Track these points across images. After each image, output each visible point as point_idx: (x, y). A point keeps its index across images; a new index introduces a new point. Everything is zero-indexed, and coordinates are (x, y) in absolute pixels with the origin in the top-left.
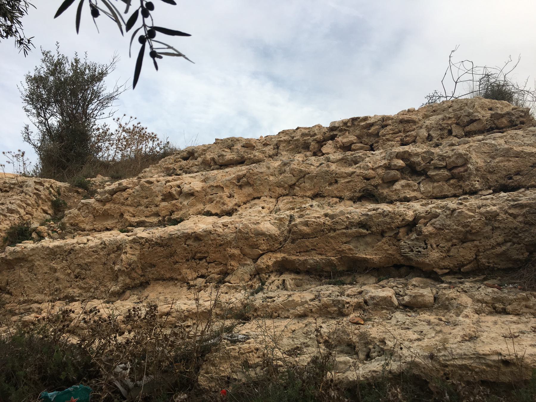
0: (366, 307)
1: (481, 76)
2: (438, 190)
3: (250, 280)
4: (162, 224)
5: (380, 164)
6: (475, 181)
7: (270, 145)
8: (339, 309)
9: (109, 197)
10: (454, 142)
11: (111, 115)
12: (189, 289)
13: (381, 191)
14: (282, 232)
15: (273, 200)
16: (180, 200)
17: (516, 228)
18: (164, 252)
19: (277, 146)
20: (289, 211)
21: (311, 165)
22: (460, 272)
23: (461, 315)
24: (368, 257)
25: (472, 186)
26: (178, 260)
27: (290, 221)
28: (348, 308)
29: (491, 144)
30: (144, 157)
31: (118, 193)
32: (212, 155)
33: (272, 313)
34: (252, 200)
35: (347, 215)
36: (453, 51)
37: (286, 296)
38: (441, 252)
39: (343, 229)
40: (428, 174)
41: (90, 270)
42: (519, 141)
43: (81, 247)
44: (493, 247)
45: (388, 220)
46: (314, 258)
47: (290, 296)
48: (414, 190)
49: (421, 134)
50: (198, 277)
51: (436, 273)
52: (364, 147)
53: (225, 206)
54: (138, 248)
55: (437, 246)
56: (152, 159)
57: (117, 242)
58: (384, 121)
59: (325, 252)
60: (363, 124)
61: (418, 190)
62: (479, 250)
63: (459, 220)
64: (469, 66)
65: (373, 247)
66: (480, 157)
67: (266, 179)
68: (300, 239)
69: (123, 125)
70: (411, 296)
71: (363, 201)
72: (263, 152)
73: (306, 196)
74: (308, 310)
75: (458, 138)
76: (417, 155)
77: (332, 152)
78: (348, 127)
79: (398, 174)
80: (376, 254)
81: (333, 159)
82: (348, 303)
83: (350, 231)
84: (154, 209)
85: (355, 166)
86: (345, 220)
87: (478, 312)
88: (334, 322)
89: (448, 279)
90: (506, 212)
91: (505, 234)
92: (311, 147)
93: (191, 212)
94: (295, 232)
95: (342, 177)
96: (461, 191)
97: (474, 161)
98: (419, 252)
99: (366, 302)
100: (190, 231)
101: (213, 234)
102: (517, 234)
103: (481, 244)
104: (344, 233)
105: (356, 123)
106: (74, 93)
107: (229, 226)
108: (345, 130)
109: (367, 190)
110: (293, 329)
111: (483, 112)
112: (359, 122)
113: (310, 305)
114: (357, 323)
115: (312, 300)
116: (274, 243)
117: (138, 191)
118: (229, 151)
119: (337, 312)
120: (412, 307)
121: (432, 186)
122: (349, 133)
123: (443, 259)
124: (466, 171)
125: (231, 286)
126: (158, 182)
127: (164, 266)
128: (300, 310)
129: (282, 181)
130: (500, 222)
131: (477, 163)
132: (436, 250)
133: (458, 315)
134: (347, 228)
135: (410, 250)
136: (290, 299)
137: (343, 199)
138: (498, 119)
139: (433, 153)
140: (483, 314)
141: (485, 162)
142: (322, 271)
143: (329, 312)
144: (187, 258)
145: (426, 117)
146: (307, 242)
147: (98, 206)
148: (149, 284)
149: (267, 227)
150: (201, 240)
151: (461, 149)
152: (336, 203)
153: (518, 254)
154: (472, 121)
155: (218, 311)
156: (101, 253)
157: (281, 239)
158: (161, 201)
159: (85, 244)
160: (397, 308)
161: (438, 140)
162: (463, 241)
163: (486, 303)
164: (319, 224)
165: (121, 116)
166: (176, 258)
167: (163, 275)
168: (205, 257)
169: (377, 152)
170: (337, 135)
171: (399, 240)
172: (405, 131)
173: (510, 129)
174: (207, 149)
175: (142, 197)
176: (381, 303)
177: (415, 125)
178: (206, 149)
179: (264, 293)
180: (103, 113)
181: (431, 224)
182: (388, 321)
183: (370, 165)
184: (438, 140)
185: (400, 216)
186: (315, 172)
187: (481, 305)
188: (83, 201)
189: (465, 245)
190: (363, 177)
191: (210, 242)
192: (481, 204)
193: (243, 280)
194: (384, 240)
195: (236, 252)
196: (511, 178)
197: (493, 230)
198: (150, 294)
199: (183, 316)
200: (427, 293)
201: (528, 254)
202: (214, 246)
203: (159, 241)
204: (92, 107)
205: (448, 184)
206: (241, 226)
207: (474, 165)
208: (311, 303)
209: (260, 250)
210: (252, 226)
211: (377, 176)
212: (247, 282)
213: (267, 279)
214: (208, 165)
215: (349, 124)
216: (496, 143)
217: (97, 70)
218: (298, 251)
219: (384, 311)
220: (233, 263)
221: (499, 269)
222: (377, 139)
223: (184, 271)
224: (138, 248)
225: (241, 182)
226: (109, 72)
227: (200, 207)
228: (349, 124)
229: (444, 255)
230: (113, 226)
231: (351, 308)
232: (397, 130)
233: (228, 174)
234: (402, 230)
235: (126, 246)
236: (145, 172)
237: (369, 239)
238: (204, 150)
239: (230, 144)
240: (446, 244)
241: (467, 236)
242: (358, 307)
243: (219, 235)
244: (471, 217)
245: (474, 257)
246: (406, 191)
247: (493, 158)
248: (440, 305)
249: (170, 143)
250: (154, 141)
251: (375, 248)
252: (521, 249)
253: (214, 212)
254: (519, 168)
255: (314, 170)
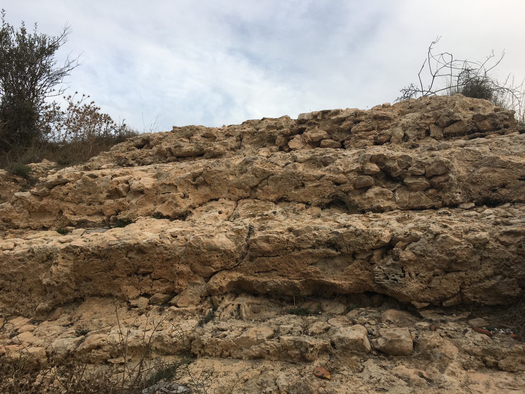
0: (334, 351)
1: (460, 71)
2: (415, 200)
3: (201, 302)
4: (107, 225)
5: (352, 168)
6: (456, 193)
7: (233, 136)
8: (302, 353)
9: (47, 190)
10: (433, 146)
11: (61, 93)
12: (129, 309)
13: (352, 198)
14: (239, 248)
15: (232, 203)
16: (128, 198)
17: (508, 260)
18: (102, 264)
19: (240, 138)
20: (249, 219)
21: (276, 164)
22: (441, 306)
23: (446, 372)
24: (337, 282)
25: (453, 198)
26: (117, 275)
27: (249, 234)
28: (311, 352)
29: (475, 151)
30: (97, 140)
31: (56, 188)
32: (168, 145)
33: (222, 352)
34: (209, 201)
35: (314, 232)
36: (434, 43)
37: (240, 329)
38: (421, 282)
39: (309, 248)
40: (405, 181)
41: (15, 281)
42: (505, 149)
43: (5, 255)
44: (481, 281)
45: (361, 241)
46: (275, 280)
47: (244, 329)
48: (389, 199)
49: (396, 133)
50: (140, 295)
51: (414, 306)
52: (334, 143)
53: (178, 208)
54: (72, 258)
55: (417, 275)
56: (105, 143)
57: (47, 250)
58: (357, 116)
59: (288, 273)
60: (334, 118)
61: (393, 199)
62: (464, 282)
63: (443, 247)
64: (448, 59)
65: (343, 271)
66: (462, 166)
67: (225, 179)
68: (260, 257)
69: (75, 103)
70: (386, 339)
71: (332, 208)
72: (225, 145)
73: (269, 200)
74: (265, 351)
75: (437, 140)
76: (393, 159)
77: (300, 147)
78: (318, 120)
79: (371, 179)
80: (346, 279)
81: (301, 158)
82: (312, 346)
83: (316, 251)
84: (98, 207)
85: (324, 169)
86: (312, 237)
87: (465, 367)
88: (294, 370)
89: (427, 314)
90: (497, 240)
91: (495, 265)
92: (278, 141)
93: (139, 212)
94: (254, 249)
95: (310, 180)
96: (441, 202)
97: (456, 170)
98: (395, 280)
99: (333, 344)
100: (132, 242)
101: (159, 247)
102: (509, 266)
103: (467, 276)
104: (310, 253)
105: (326, 116)
106: (21, 68)
107: (179, 237)
108: (315, 123)
109: (337, 196)
110: (245, 378)
111: (464, 112)
112: (330, 115)
113: (267, 345)
114: (322, 377)
115: (270, 338)
116: (229, 260)
117: (79, 186)
118: (187, 140)
119: (299, 356)
120: (388, 353)
121: (408, 196)
122: (318, 127)
123: (423, 291)
124: (447, 180)
125: (178, 311)
126: (103, 175)
127: (101, 281)
128: (255, 350)
129: (243, 182)
130: (489, 250)
131: (459, 172)
132: (415, 280)
133: (442, 371)
134: (313, 247)
135: (384, 277)
136: (244, 335)
137: (310, 205)
138: (480, 121)
139: (411, 158)
140: (472, 370)
141: (468, 171)
142: (284, 295)
143: (290, 356)
144: (128, 273)
145: (402, 114)
146: (267, 261)
147: (34, 200)
148: (84, 301)
149: (221, 242)
150: (144, 253)
151: (442, 155)
152: (302, 209)
153: (508, 290)
154: (452, 122)
155: (158, 345)
156: (29, 263)
157: (238, 256)
158: (105, 199)
159: (11, 250)
160: (369, 353)
161: (414, 140)
162: (446, 272)
163: (475, 355)
164: (281, 241)
165: (72, 94)
166: (116, 273)
167: (100, 291)
168: (150, 273)
169: (348, 152)
170: (305, 128)
171: (372, 264)
172: (379, 129)
173: (493, 133)
174: (164, 138)
175: (84, 193)
176: (351, 347)
177: (390, 122)
178: (163, 137)
179: (215, 324)
180: (54, 90)
181: (410, 249)
182: (360, 375)
183: (341, 168)
184: (414, 140)
185: (375, 236)
186: (280, 174)
187: (468, 357)
188: (17, 194)
189: (449, 275)
190: (333, 181)
191: (156, 256)
192: (468, 228)
193: (192, 303)
194: (356, 263)
195: (185, 269)
196: (494, 191)
197: (481, 260)
198: (84, 314)
199: (116, 351)
200: (404, 336)
201: (520, 289)
202: (160, 260)
203: (95, 252)
204: (40, 82)
205: (426, 194)
206: (191, 239)
207: (455, 175)
208: (269, 342)
209: (213, 267)
210: (206, 240)
211: (348, 182)
212: (197, 305)
213: (220, 302)
214: (165, 156)
215: (319, 118)
216: (480, 151)
217: (47, 41)
218: (257, 271)
219: (354, 357)
220: (181, 282)
221: (486, 306)
222: (348, 136)
223: (124, 287)
224: (72, 258)
225: (198, 181)
226: (60, 43)
227: (150, 207)
228: (319, 118)
229: (424, 286)
230: (51, 224)
231: (315, 352)
232: (370, 127)
233: (182, 171)
234: (376, 253)
235: (58, 256)
236: (93, 160)
237: (338, 261)
238: (160, 139)
239: (189, 132)
240: (427, 273)
241: (451, 265)
242: (324, 350)
243: (166, 249)
244: (457, 243)
245: (459, 290)
246: (380, 200)
247: (477, 167)
248: (420, 353)
249: (127, 125)
250: (108, 123)
251: (345, 271)
252: (513, 284)
253: (165, 213)
254: (505, 180)
255: (278, 170)
